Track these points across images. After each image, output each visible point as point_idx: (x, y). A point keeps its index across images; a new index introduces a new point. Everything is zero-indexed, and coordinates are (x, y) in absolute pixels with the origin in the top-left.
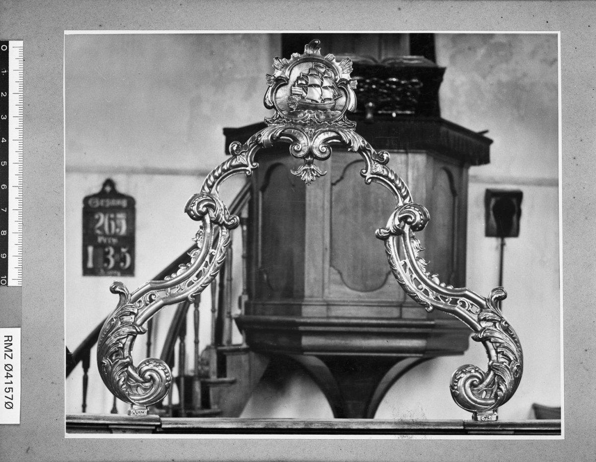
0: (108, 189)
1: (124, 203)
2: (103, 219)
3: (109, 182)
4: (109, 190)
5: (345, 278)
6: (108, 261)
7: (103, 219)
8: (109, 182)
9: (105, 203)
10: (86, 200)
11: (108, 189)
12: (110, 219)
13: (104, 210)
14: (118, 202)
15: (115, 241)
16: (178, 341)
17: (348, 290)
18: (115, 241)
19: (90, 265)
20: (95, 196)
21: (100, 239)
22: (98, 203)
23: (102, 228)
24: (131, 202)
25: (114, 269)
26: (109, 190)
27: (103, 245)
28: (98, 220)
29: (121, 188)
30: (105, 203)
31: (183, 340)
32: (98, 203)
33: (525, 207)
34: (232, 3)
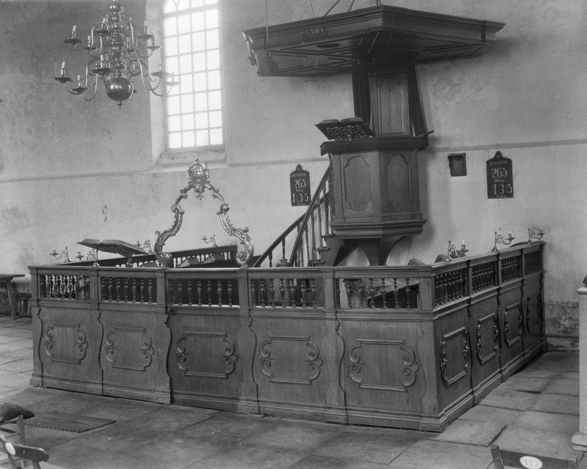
0: (299, 169)
1: (305, 175)
2: (298, 182)
3: (299, 166)
4: (299, 169)
5: (352, 206)
6: (301, 200)
7: (496, 171)
8: (299, 166)
9: (298, 175)
10: (488, 162)
11: (299, 169)
12: (300, 182)
13: (496, 167)
14: (302, 174)
15: (503, 181)
16: (305, 233)
17: (353, 211)
18: (503, 181)
19: (294, 202)
20: (294, 172)
21: (496, 181)
22: (295, 175)
23: (496, 175)
24: (307, 173)
25: (504, 194)
26: (299, 169)
27: (298, 193)
28: (494, 171)
29: (304, 169)
30: (298, 175)
31: (307, 233)
32: (295, 175)
33: (463, 177)
34: (388, 91)
